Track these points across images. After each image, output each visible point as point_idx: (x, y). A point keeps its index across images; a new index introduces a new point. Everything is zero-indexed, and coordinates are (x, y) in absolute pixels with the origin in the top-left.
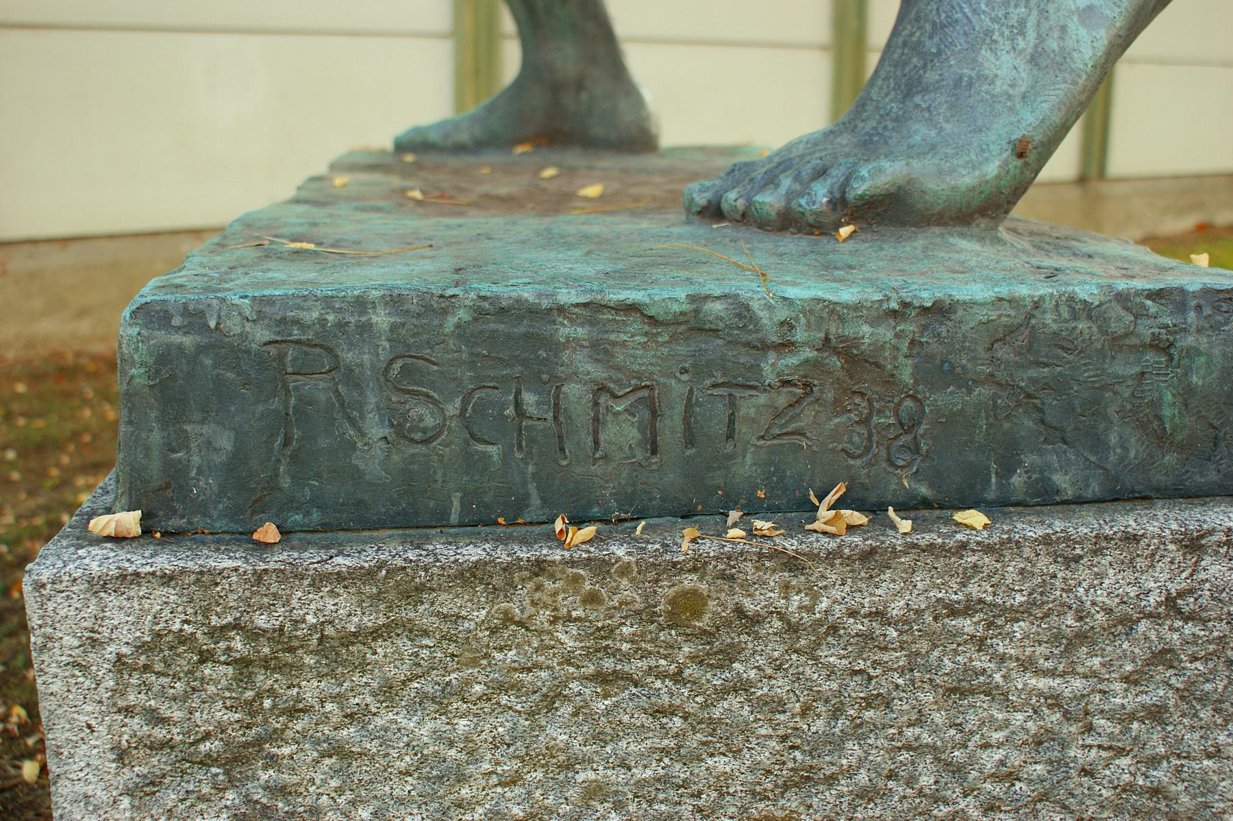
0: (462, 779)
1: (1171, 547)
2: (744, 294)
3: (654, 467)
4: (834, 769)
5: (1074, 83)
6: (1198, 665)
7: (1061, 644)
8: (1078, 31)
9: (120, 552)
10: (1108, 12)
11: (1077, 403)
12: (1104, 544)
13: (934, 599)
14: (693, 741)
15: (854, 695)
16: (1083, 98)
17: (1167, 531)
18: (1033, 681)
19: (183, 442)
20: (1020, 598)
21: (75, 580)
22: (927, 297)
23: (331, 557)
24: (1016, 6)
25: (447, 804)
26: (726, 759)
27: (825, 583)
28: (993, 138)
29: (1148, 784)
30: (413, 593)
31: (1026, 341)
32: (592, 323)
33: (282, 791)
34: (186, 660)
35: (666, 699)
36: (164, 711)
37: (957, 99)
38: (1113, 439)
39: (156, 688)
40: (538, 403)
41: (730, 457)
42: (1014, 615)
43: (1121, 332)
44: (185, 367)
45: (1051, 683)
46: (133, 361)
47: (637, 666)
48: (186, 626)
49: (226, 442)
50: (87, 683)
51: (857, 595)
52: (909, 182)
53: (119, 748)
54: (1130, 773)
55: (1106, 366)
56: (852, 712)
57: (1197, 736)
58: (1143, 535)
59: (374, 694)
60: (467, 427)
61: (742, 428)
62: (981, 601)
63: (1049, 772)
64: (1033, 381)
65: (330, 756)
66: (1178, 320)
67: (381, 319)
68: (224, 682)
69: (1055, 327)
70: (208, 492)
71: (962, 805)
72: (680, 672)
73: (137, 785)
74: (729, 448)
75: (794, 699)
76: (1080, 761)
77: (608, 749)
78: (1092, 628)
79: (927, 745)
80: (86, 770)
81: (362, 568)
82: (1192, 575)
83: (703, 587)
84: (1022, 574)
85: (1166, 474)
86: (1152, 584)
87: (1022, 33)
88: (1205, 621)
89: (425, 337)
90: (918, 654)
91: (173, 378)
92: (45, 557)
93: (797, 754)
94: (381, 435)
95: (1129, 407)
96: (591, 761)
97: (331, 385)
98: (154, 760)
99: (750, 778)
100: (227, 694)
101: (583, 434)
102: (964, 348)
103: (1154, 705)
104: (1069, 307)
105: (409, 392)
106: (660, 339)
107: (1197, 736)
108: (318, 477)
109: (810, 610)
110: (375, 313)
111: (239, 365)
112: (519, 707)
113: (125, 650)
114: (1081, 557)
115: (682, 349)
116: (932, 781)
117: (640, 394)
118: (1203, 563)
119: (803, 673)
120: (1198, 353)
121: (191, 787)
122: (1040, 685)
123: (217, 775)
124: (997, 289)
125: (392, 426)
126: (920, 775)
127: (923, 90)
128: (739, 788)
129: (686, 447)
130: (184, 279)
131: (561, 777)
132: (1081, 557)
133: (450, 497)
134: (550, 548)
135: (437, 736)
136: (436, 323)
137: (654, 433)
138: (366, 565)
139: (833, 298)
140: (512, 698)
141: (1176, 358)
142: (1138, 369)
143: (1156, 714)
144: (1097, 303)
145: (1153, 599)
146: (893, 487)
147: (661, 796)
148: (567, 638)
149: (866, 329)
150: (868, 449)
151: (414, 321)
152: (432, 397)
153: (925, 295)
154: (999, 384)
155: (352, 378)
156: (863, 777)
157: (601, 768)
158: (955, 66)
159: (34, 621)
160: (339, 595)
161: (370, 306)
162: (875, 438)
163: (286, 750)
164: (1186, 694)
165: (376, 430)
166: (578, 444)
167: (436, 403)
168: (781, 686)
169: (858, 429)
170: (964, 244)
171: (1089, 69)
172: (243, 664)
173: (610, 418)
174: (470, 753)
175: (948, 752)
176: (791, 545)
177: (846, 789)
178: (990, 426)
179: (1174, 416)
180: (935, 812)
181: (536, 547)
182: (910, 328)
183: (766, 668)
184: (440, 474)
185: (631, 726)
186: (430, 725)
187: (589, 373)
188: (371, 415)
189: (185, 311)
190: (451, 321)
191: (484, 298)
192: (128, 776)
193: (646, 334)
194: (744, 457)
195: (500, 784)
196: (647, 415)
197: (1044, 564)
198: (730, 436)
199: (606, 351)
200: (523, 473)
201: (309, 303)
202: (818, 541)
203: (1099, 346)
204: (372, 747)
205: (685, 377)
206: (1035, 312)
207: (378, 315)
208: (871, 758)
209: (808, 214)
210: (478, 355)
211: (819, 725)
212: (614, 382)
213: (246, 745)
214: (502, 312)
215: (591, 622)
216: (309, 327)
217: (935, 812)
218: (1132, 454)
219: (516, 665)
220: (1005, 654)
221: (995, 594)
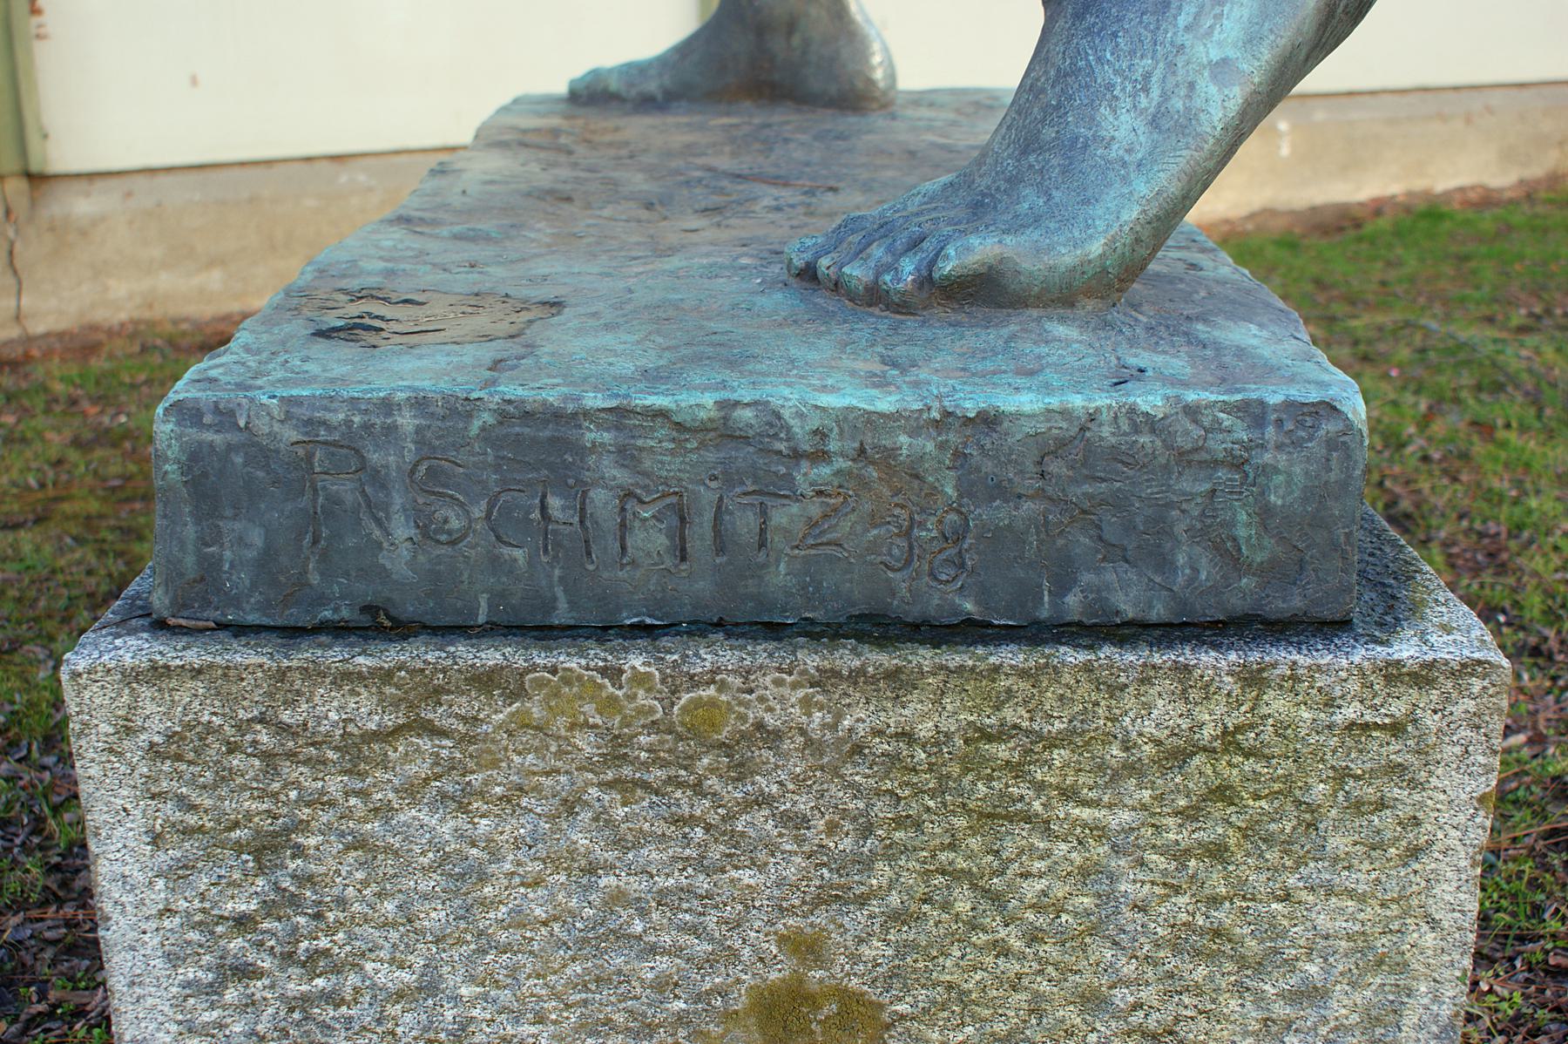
0: (483, 878)
1: (1229, 679)
2: (776, 402)
3: (684, 574)
4: (863, 889)
5: (1199, 149)
6: (1263, 803)
7: (1105, 774)
8: (1207, 88)
9: (155, 644)
10: (1245, 66)
11: (1139, 520)
12: (1152, 673)
13: (964, 723)
14: (716, 852)
15: (880, 815)
16: (1211, 164)
17: (1223, 662)
18: (1077, 811)
19: (217, 539)
20: (1058, 725)
21: (109, 670)
22: (970, 407)
23: (353, 657)
24: (1142, 57)
25: (470, 901)
26: (752, 873)
27: (848, 701)
28: (1100, 212)
29: (1208, 925)
30: (435, 694)
31: (1080, 455)
32: (618, 428)
33: (306, 880)
34: (215, 747)
35: (686, 810)
37: (1071, 164)
38: (1181, 559)
39: (187, 777)
40: (564, 508)
41: (764, 566)
43: (1189, 446)
44: (216, 465)
45: (1097, 814)
46: (167, 457)
47: (657, 775)
48: (214, 718)
49: (256, 537)
50: (123, 768)
51: (883, 714)
52: (1001, 261)
53: (154, 832)
54: (1188, 912)
55: (1172, 482)
56: (880, 832)
57: (1263, 878)
58: (1195, 665)
59: (396, 791)
60: (493, 530)
61: (775, 539)
62: (1015, 726)
63: (1097, 906)
64: (1090, 497)
65: (356, 849)
66: (1255, 435)
67: (407, 421)
68: (251, 774)
69: (1113, 440)
70: (241, 586)
71: (1002, 933)
72: (699, 784)
73: (171, 867)
74: (761, 557)
75: (819, 815)
76: (1132, 896)
77: (630, 856)
78: (1140, 759)
79: (962, 870)
80: (123, 851)
81: (381, 668)
82: (1252, 709)
84: (1061, 700)
85: (1244, 598)
86: (1207, 717)
87: (1146, 90)
88: (1268, 758)
89: (451, 439)
90: (948, 777)
91: (205, 475)
92: (84, 646)
93: (825, 871)
94: (406, 536)
95: (1199, 526)
96: (613, 867)
97: (358, 485)
98: (187, 845)
99: (776, 893)
100: (255, 785)
101: (610, 538)
102: (1010, 461)
103: (1211, 843)
104: (1129, 419)
105: (434, 493)
106: (689, 446)
107: (1263, 878)
108: (347, 574)
109: (834, 727)
110: (400, 415)
111: (268, 465)
112: (539, 810)
113: (157, 739)
114: (1126, 686)
115: (711, 456)
116: (968, 908)
117: (668, 501)
118: (1265, 697)
119: (827, 790)
120: (1276, 471)
121: (223, 872)
122: (1084, 816)
123: (247, 861)
124: (1046, 401)
125: (418, 527)
126: (955, 900)
127: (1040, 148)
128: (765, 902)
129: (717, 555)
130: (221, 370)
131: (584, 881)
132: (1126, 686)
133: (476, 598)
134: (568, 654)
135: (459, 834)
136: (461, 425)
137: (683, 539)
138: (386, 666)
139: (871, 408)
140: (533, 801)
141: (1251, 475)
142: (1207, 486)
143: (1217, 852)
144: (1161, 416)
145: (1208, 732)
146: (936, 602)
147: (685, 906)
148: (586, 744)
149: (904, 439)
150: (908, 562)
151: (439, 423)
152: (457, 499)
153: (968, 405)
154: (1050, 499)
155: (378, 478)
156: (894, 899)
157: (623, 874)
159: (73, 709)
160: (359, 694)
161: (396, 408)
162: (916, 551)
163: (312, 841)
164: (1250, 833)
165: (402, 530)
166: (605, 548)
167: (462, 505)
168: (804, 804)
169: (898, 541)
170: (1060, 330)
171: (1217, 133)
172: (267, 756)
173: (637, 524)
174: (491, 854)
175: (986, 878)
177: (877, 910)
178: (1041, 542)
179: (1250, 537)
180: (974, 939)
181: (555, 652)
182: (953, 438)
183: (787, 783)
184: (466, 575)
185: (652, 834)
186: (451, 823)
187: (615, 478)
188: (397, 516)
189: (216, 409)
190: (476, 425)
191: (510, 402)
192: (163, 858)
193: (673, 440)
194: (778, 566)
195: (522, 884)
196: (675, 521)
197: (1085, 689)
198: (762, 544)
199: (633, 457)
200: (549, 576)
201: (335, 405)
202: (841, 658)
203: (1164, 461)
204: (396, 842)
205: (713, 485)
206: (1089, 425)
207: (403, 417)
208: (902, 880)
209: (892, 293)
210: (503, 458)
211: (847, 844)
212: (641, 487)
213: (275, 834)
214: (527, 416)
215: (608, 729)
216: (335, 428)
217: (974, 939)
218: (1203, 576)
219: (535, 768)
220: (1043, 781)
221: (1031, 720)
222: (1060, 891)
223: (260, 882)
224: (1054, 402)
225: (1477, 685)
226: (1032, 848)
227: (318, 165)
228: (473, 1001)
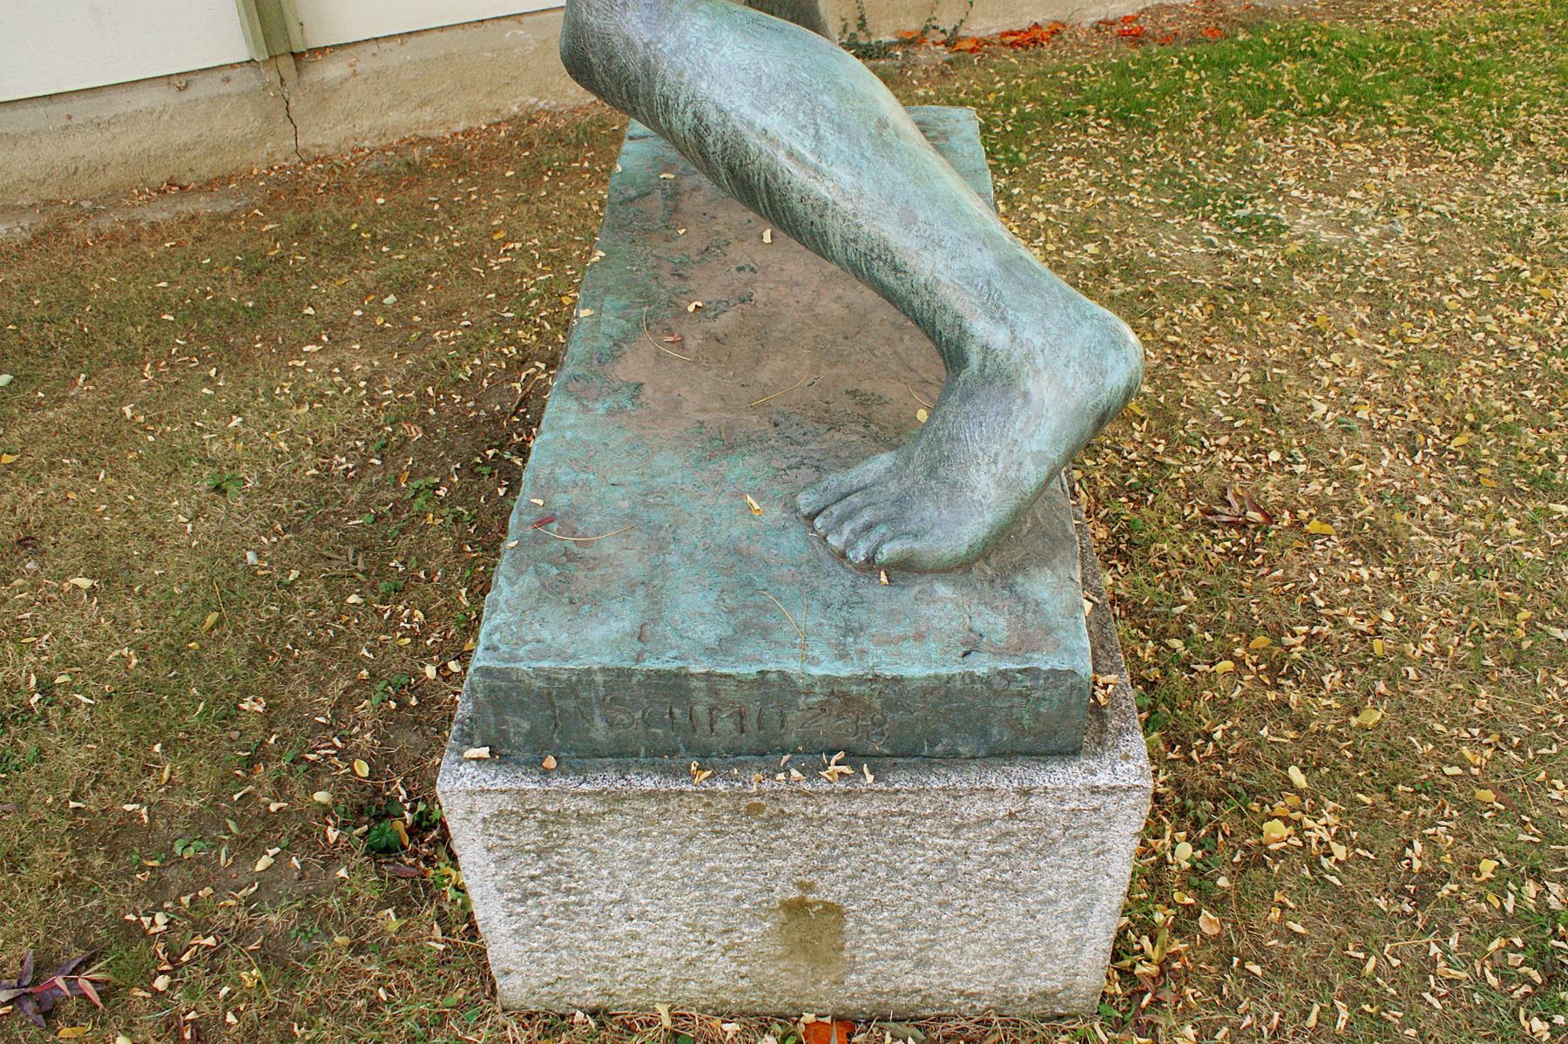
0: (649, 863)
36: (507, 836)
40: (682, 714)
42: (927, 817)
83: (763, 802)
87: (995, 463)
109: (818, 812)
143: (1006, 855)
149: (854, 688)
156: (849, 871)
158: (954, 474)
165: (600, 724)
168: (805, 838)
176: (808, 787)
186: (632, 845)
197: (943, 798)
222: (927, 868)
223: (541, 863)
224: (931, 672)
225: (1136, 794)
226: (916, 854)
227: (488, 24)
228: (647, 905)
